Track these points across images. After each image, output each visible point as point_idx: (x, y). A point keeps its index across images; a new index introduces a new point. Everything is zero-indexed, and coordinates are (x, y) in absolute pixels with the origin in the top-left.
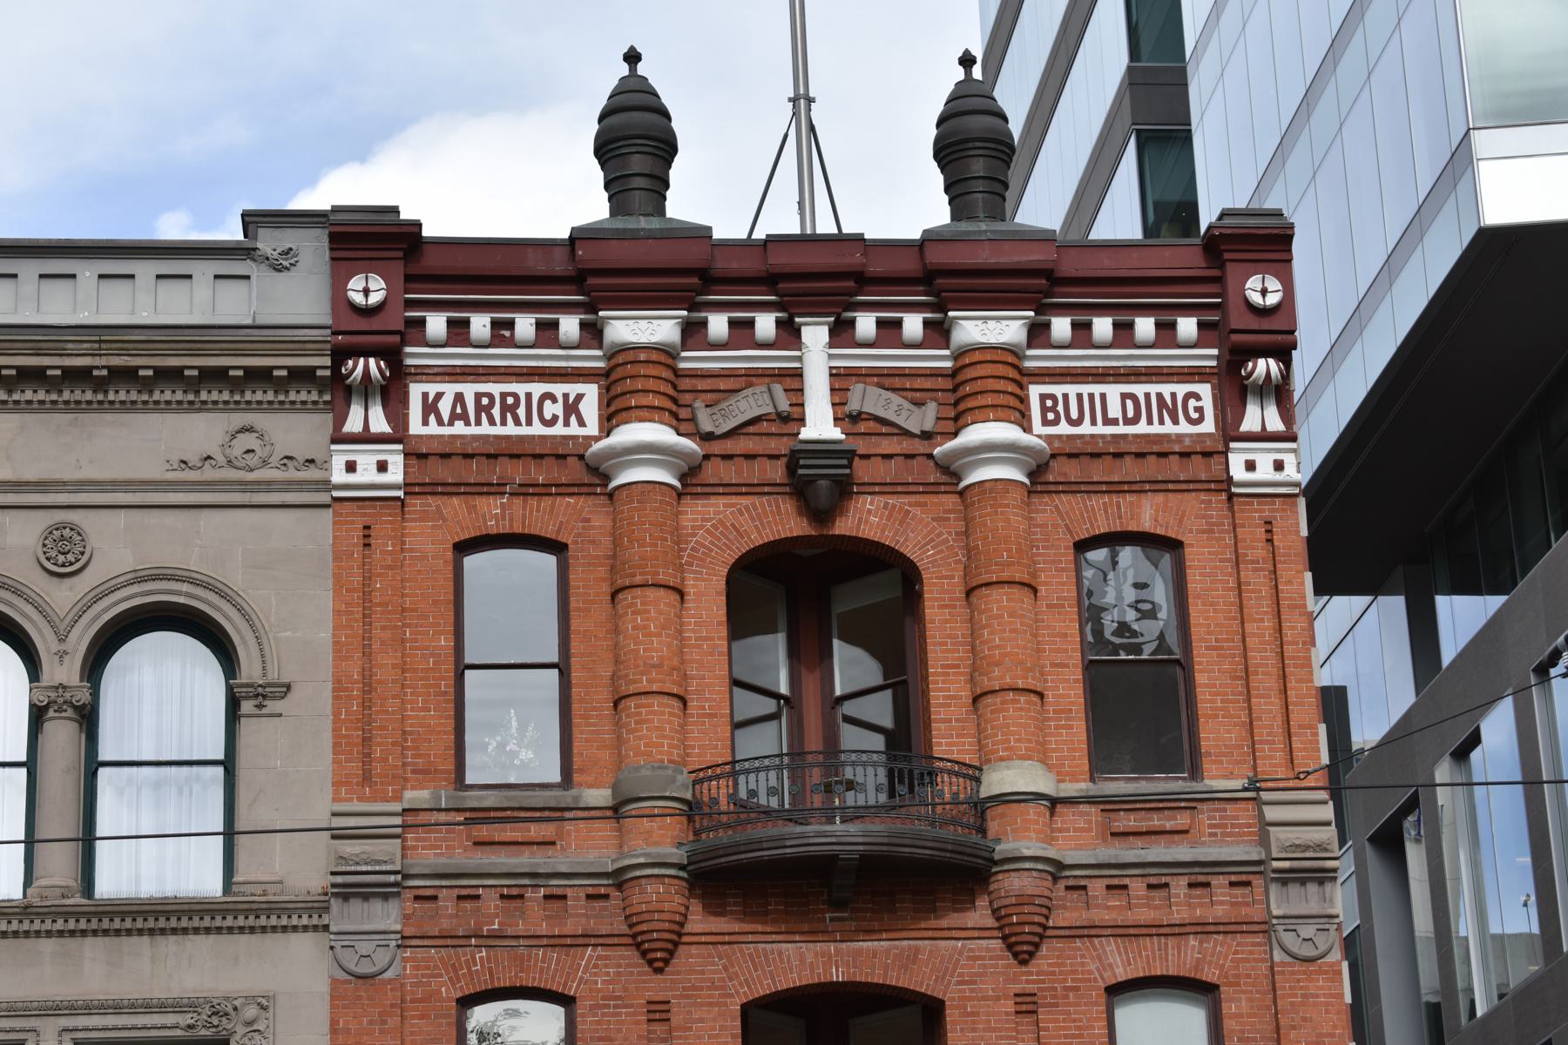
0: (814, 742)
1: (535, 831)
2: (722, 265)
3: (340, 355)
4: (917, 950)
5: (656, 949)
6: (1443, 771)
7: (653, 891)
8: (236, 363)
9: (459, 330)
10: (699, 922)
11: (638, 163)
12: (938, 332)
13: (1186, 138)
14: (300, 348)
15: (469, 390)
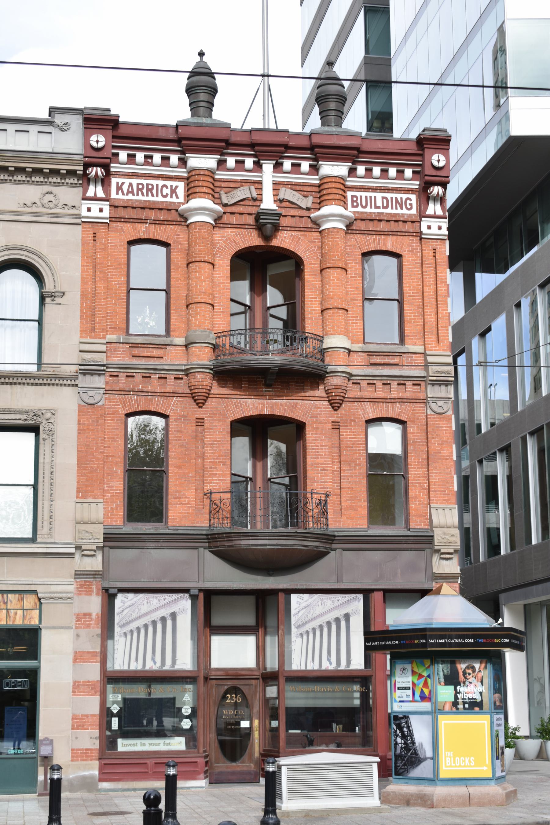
0: (258, 324)
2: (234, 138)
3: (86, 166)
4: (297, 404)
5: (200, 399)
6: (475, 341)
10: (216, 389)
11: (203, 96)
12: (315, 169)
15: (135, 182)
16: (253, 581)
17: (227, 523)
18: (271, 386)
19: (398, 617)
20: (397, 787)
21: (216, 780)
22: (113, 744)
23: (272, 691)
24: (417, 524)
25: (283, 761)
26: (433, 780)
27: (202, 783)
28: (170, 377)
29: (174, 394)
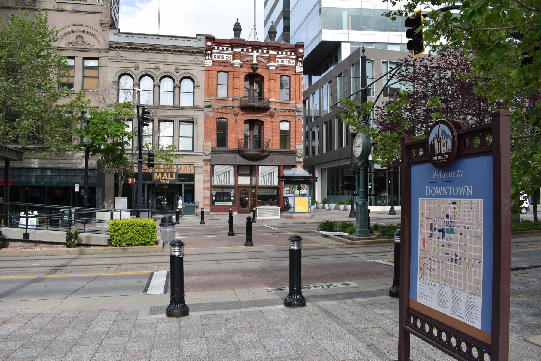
0: (252, 95)
1: (225, 102)
2: (246, 43)
3: (206, 51)
5: (236, 115)
6: (311, 96)
7: (236, 109)
8: (195, 51)
9: (218, 48)
10: (240, 112)
11: (238, 32)
12: (268, 52)
13: (289, 19)
14: (202, 50)
15: (219, 55)
16: (249, 161)
17: (243, 148)
18: (255, 110)
19: (287, 173)
20: (284, 214)
21: (239, 212)
22: (213, 203)
23: (254, 191)
24: (292, 148)
25: (257, 208)
26: (294, 213)
27: (236, 213)
28: (228, 109)
29: (229, 113)
